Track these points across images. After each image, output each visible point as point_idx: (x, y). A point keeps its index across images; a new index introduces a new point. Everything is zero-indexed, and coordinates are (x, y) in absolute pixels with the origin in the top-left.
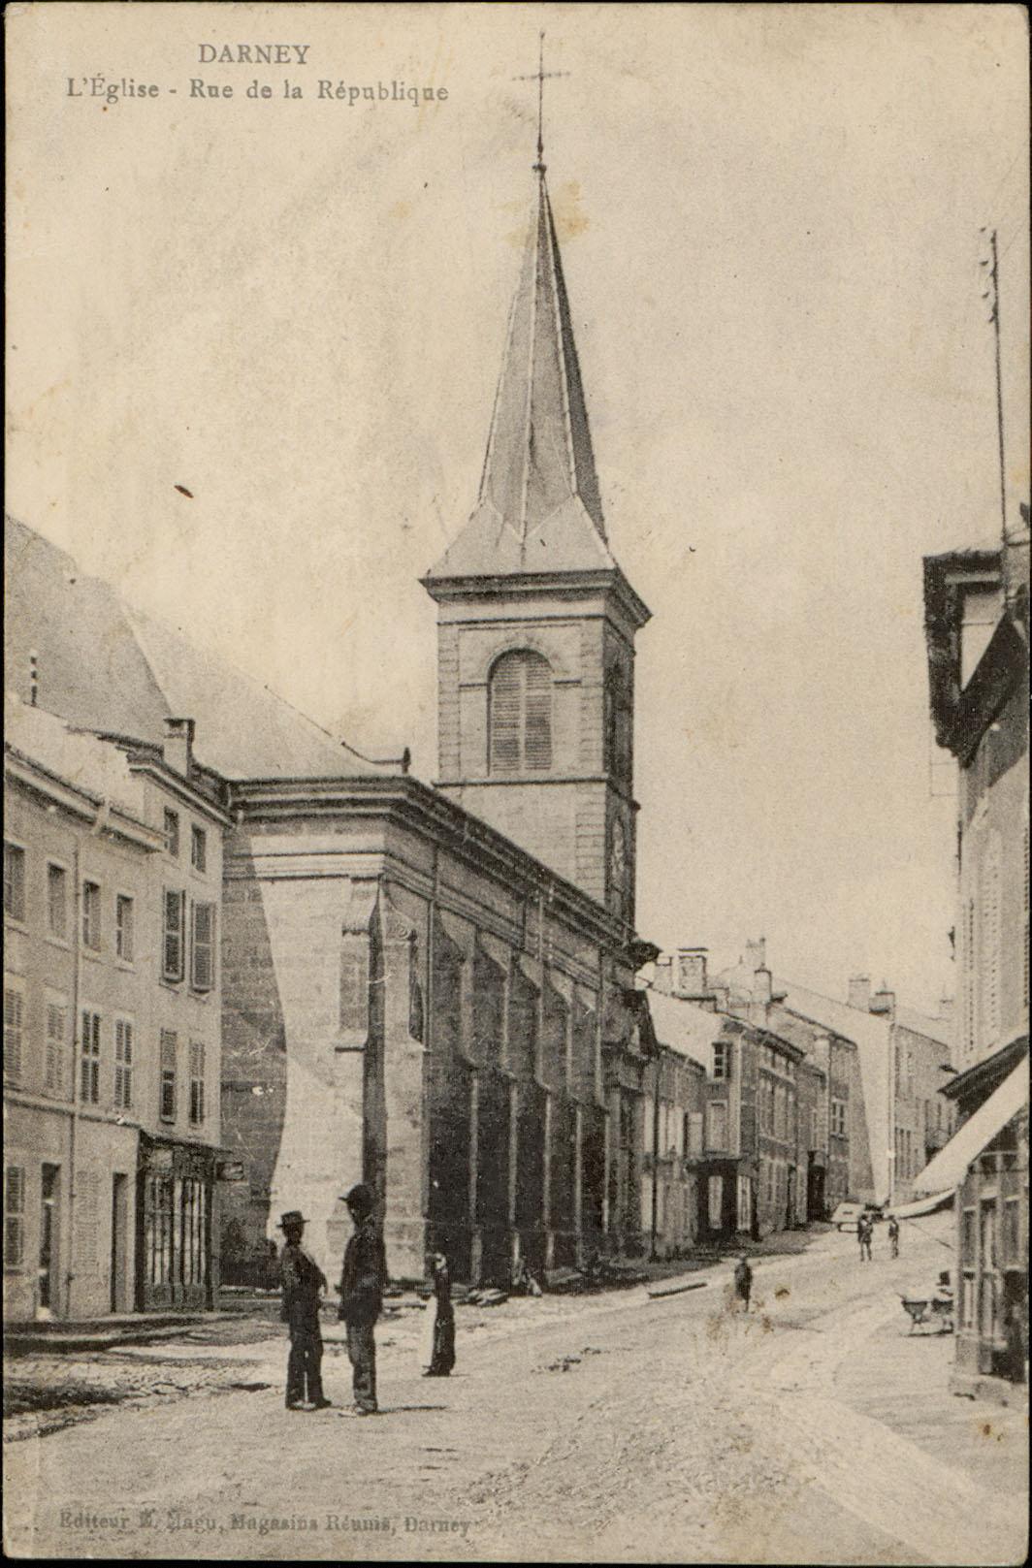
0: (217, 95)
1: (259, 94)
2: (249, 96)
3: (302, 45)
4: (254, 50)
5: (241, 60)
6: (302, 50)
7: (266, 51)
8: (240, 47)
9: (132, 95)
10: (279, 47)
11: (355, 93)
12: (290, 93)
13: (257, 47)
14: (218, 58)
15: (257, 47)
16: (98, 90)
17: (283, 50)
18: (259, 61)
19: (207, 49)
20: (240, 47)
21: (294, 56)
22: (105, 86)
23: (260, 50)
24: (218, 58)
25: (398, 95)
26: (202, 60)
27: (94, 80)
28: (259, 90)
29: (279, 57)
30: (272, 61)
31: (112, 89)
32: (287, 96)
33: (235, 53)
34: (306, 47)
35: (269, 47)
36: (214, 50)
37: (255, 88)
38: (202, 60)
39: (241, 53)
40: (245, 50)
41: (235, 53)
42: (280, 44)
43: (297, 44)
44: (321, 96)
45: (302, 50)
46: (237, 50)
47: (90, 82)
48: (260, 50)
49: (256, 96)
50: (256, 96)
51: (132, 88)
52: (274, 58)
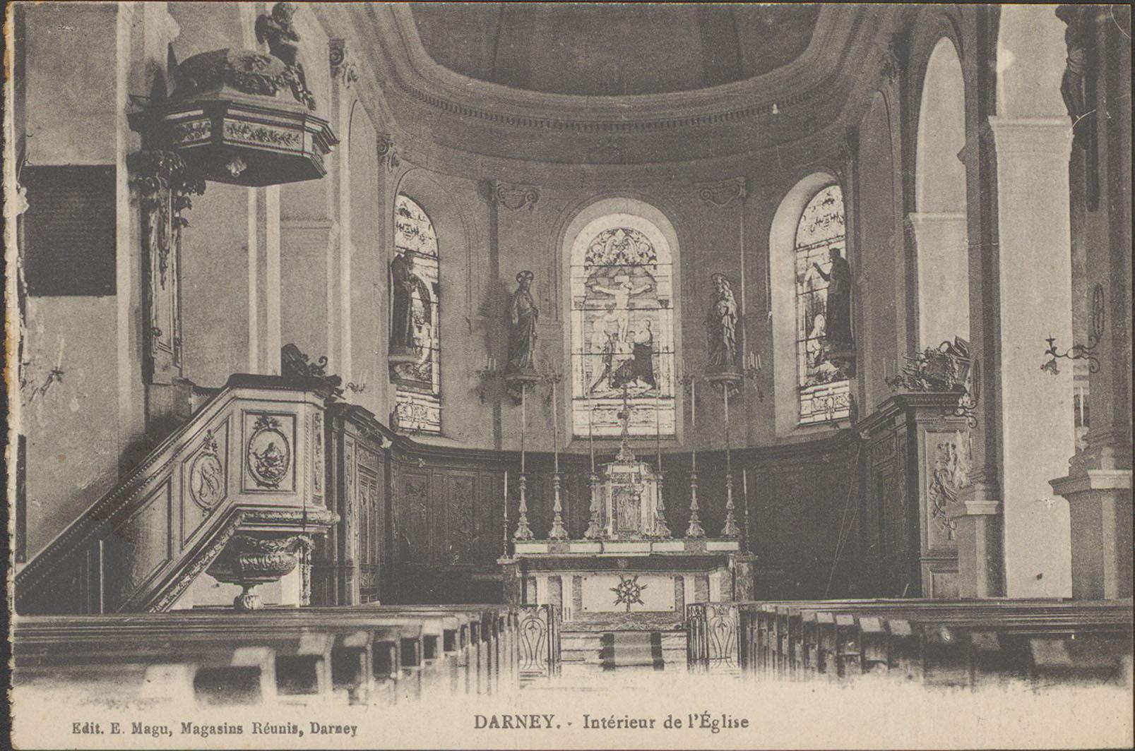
0: (645, 726)
1: (673, 725)
2: (665, 726)
3: (548, 714)
4: (515, 719)
5: (505, 727)
6: (549, 718)
7: (523, 718)
8: (505, 717)
9: (289, 732)
10: (532, 717)
11: (668, 724)
12: (590, 724)
13: (517, 716)
14: (488, 724)
15: (517, 716)
16: (706, 724)
17: (535, 718)
18: (518, 727)
19: (480, 718)
20: (505, 717)
21: (543, 722)
22: (710, 722)
23: (518, 718)
24: (488, 724)
25: (727, 724)
26: (477, 727)
27: (702, 716)
28: (673, 721)
29: (532, 723)
30: (528, 727)
31: (716, 722)
32: (587, 727)
33: (501, 722)
34: (552, 716)
35: (525, 716)
36: (485, 719)
37: (670, 721)
38: (477, 727)
39: (505, 722)
40: (508, 719)
41: (501, 722)
42: (532, 714)
43: (545, 714)
44: (255, 732)
45: (494, 725)
46: (502, 718)
47: (700, 718)
48: (518, 718)
49: (671, 727)
50: (671, 727)
51: (730, 721)
52: (529, 723)
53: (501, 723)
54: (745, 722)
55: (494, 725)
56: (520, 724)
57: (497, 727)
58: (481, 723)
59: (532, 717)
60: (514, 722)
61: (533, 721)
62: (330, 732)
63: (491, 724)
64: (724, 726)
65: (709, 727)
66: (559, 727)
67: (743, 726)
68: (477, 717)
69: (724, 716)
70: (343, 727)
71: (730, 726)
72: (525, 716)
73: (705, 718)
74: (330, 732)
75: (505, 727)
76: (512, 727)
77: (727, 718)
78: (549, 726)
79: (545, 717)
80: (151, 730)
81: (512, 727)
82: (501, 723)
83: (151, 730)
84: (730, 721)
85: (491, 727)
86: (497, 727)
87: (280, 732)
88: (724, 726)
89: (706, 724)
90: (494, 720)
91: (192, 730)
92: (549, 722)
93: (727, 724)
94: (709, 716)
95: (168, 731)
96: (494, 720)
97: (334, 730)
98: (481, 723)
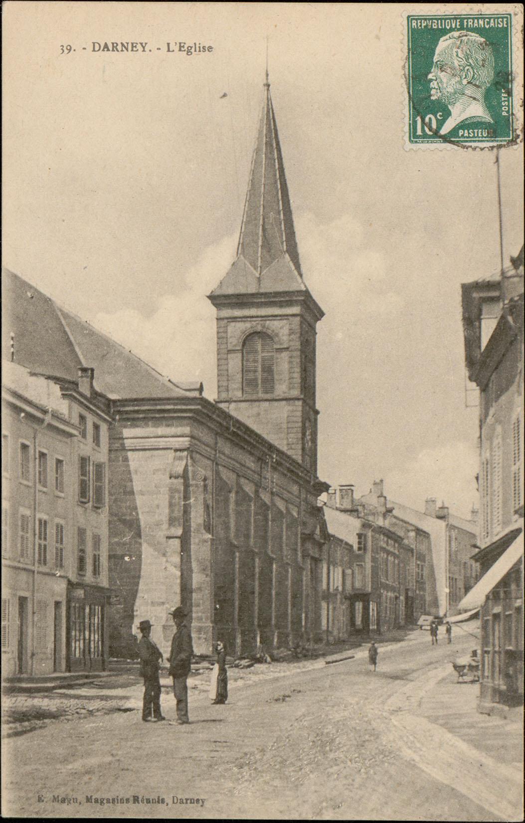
4: (120, 45)
6: (144, 45)
7: (126, 45)
8: (113, 44)
15: (122, 43)
17: (134, 45)
18: (122, 51)
20: (113, 44)
25: (198, 49)
26: (94, 50)
31: (189, 48)
34: (146, 44)
35: (128, 43)
38: (94, 50)
39: (113, 46)
40: (115, 45)
51: (200, 47)
53: (111, 48)
54: (210, 48)
55: (106, 49)
56: (124, 49)
57: (108, 50)
58: (97, 48)
59: (132, 44)
60: (119, 47)
61: (133, 47)
62: (187, 803)
63: (104, 48)
64: (195, 51)
65: (185, 51)
66: (150, 51)
67: (209, 51)
68: (94, 43)
69: (195, 44)
70: (207, 47)
71: (200, 51)
72: (128, 43)
73: (182, 45)
74: (187, 803)
75: (113, 50)
76: (118, 51)
77: (197, 46)
78: (144, 51)
79: (141, 44)
80: (99, 801)
81: (118, 51)
82: (111, 48)
83: (99, 801)
84: (200, 47)
85: (103, 50)
86: (108, 50)
87: (153, 803)
88: (195, 51)
89: (182, 49)
90: (106, 46)
91: (93, 801)
92: (144, 48)
93: (198, 49)
94: (185, 43)
95: (78, 801)
96: (106, 46)
97: (189, 801)
98: (97, 48)
